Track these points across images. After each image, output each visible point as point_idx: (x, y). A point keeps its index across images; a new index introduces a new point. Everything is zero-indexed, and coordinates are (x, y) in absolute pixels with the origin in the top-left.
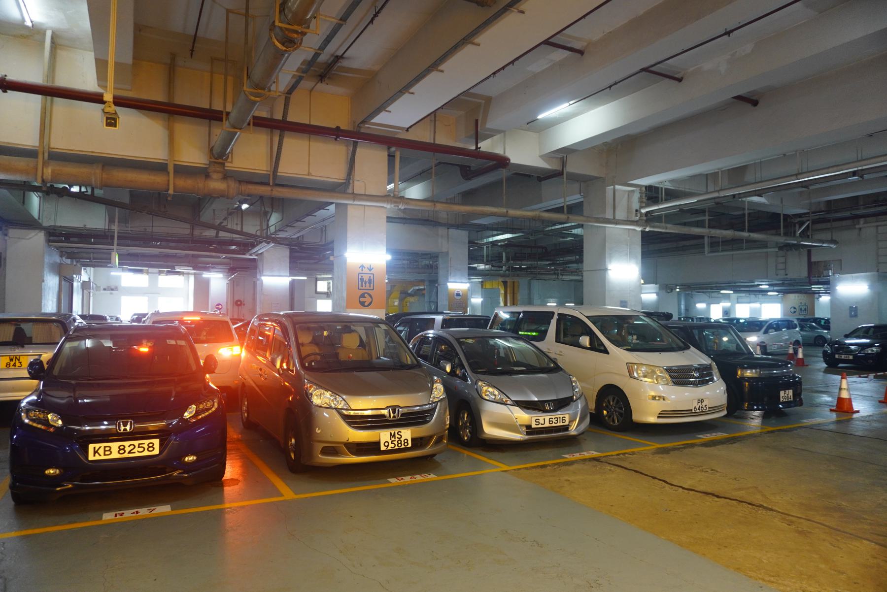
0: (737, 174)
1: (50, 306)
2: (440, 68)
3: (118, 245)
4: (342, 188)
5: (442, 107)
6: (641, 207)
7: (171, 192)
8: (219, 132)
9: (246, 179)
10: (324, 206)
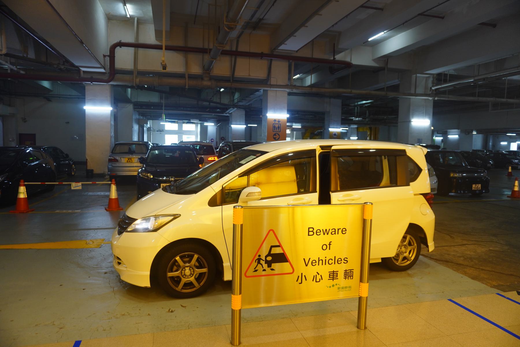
0: (500, 63)
1: (135, 138)
2: (295, 35)
3: (165, 110)
4: (265, 82)
5: (315, 38)
6: (433, 86)
7: (187, 87)
8: (207, 57)
9: (220, 80)
10: (258, 90)
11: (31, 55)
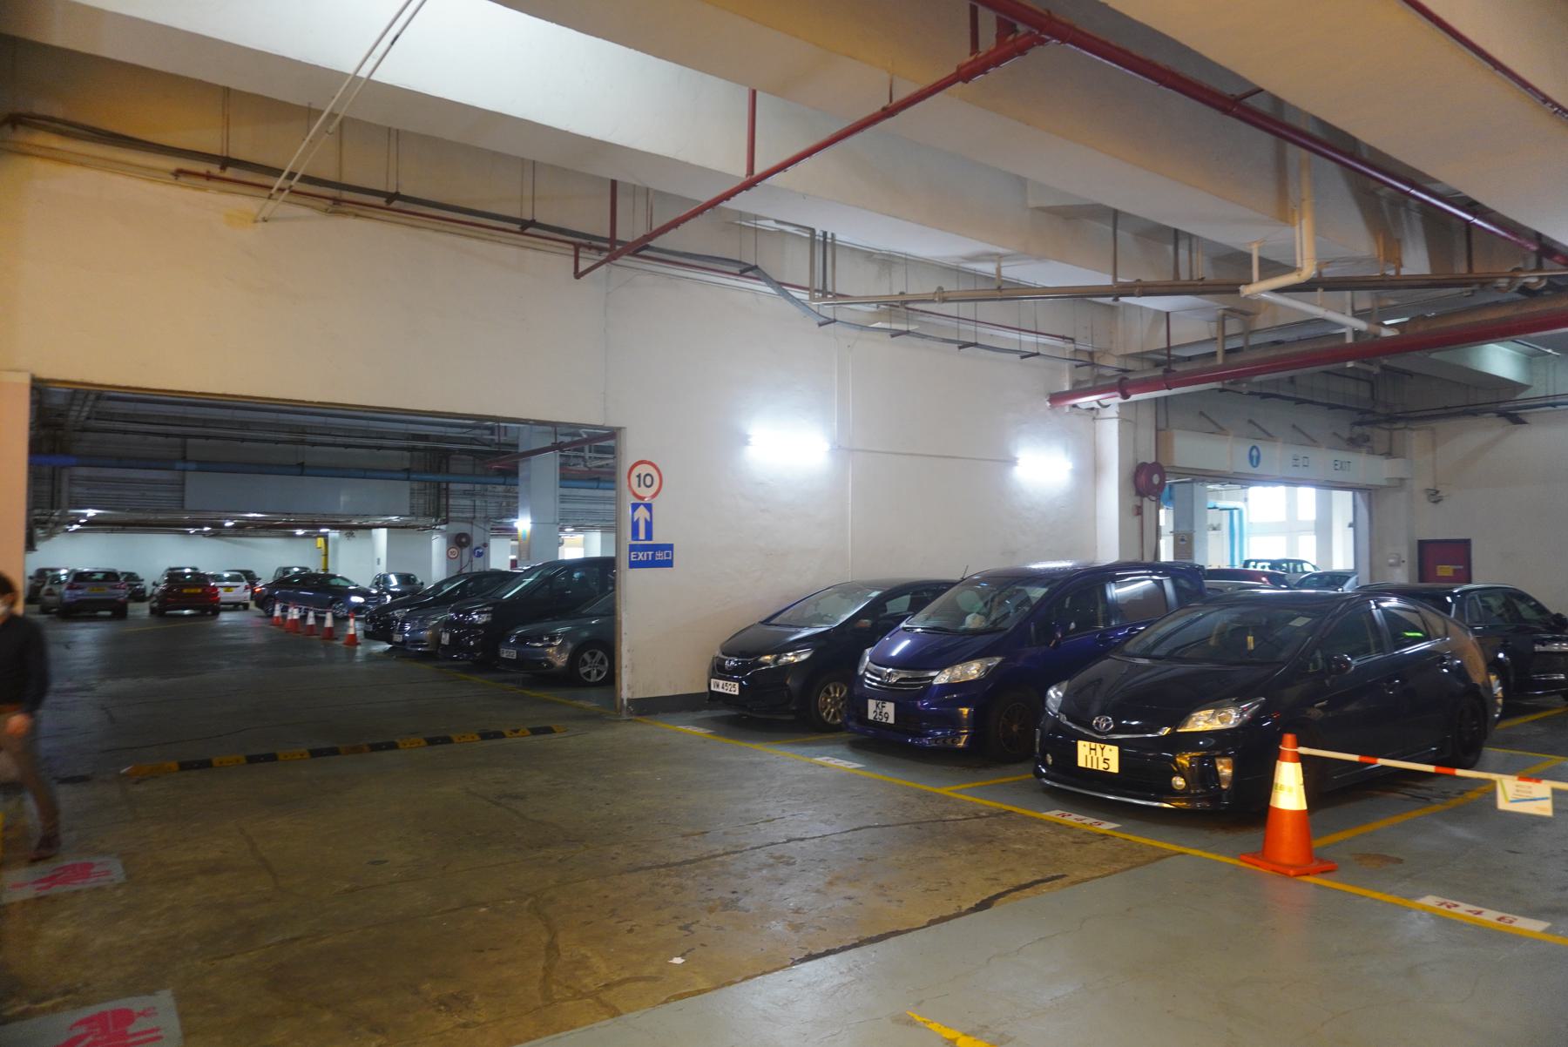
11: (1416, 262)
